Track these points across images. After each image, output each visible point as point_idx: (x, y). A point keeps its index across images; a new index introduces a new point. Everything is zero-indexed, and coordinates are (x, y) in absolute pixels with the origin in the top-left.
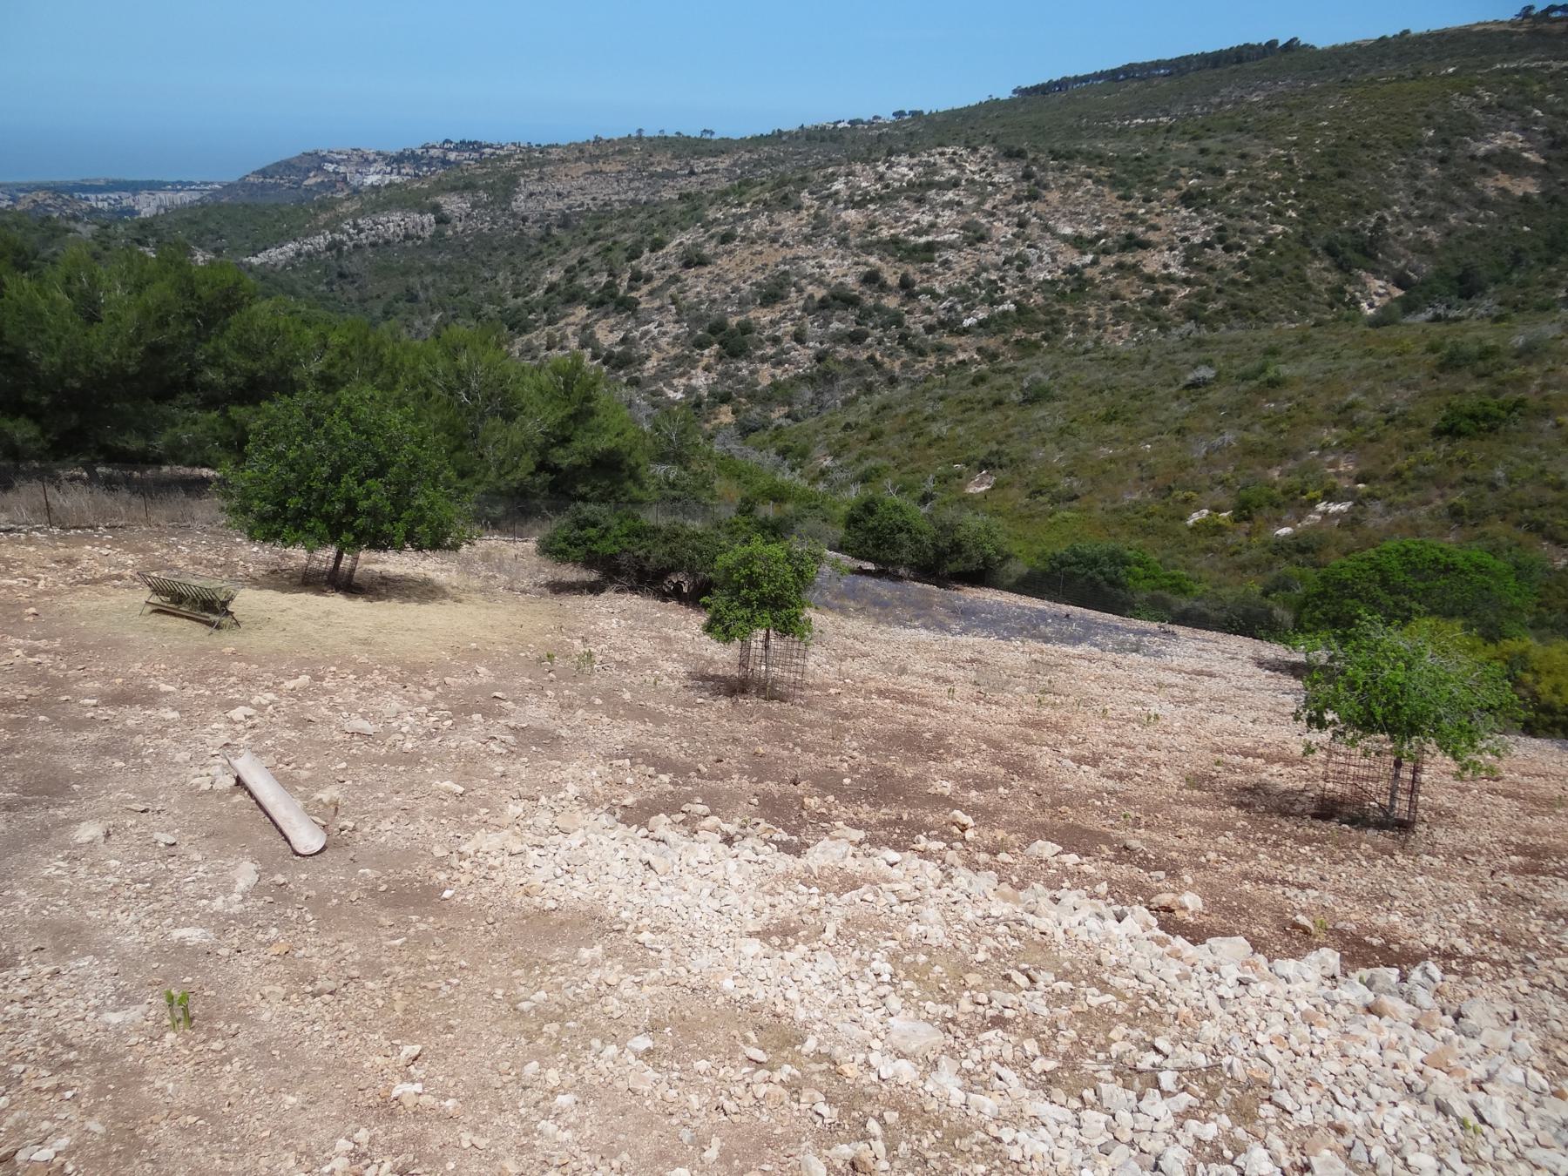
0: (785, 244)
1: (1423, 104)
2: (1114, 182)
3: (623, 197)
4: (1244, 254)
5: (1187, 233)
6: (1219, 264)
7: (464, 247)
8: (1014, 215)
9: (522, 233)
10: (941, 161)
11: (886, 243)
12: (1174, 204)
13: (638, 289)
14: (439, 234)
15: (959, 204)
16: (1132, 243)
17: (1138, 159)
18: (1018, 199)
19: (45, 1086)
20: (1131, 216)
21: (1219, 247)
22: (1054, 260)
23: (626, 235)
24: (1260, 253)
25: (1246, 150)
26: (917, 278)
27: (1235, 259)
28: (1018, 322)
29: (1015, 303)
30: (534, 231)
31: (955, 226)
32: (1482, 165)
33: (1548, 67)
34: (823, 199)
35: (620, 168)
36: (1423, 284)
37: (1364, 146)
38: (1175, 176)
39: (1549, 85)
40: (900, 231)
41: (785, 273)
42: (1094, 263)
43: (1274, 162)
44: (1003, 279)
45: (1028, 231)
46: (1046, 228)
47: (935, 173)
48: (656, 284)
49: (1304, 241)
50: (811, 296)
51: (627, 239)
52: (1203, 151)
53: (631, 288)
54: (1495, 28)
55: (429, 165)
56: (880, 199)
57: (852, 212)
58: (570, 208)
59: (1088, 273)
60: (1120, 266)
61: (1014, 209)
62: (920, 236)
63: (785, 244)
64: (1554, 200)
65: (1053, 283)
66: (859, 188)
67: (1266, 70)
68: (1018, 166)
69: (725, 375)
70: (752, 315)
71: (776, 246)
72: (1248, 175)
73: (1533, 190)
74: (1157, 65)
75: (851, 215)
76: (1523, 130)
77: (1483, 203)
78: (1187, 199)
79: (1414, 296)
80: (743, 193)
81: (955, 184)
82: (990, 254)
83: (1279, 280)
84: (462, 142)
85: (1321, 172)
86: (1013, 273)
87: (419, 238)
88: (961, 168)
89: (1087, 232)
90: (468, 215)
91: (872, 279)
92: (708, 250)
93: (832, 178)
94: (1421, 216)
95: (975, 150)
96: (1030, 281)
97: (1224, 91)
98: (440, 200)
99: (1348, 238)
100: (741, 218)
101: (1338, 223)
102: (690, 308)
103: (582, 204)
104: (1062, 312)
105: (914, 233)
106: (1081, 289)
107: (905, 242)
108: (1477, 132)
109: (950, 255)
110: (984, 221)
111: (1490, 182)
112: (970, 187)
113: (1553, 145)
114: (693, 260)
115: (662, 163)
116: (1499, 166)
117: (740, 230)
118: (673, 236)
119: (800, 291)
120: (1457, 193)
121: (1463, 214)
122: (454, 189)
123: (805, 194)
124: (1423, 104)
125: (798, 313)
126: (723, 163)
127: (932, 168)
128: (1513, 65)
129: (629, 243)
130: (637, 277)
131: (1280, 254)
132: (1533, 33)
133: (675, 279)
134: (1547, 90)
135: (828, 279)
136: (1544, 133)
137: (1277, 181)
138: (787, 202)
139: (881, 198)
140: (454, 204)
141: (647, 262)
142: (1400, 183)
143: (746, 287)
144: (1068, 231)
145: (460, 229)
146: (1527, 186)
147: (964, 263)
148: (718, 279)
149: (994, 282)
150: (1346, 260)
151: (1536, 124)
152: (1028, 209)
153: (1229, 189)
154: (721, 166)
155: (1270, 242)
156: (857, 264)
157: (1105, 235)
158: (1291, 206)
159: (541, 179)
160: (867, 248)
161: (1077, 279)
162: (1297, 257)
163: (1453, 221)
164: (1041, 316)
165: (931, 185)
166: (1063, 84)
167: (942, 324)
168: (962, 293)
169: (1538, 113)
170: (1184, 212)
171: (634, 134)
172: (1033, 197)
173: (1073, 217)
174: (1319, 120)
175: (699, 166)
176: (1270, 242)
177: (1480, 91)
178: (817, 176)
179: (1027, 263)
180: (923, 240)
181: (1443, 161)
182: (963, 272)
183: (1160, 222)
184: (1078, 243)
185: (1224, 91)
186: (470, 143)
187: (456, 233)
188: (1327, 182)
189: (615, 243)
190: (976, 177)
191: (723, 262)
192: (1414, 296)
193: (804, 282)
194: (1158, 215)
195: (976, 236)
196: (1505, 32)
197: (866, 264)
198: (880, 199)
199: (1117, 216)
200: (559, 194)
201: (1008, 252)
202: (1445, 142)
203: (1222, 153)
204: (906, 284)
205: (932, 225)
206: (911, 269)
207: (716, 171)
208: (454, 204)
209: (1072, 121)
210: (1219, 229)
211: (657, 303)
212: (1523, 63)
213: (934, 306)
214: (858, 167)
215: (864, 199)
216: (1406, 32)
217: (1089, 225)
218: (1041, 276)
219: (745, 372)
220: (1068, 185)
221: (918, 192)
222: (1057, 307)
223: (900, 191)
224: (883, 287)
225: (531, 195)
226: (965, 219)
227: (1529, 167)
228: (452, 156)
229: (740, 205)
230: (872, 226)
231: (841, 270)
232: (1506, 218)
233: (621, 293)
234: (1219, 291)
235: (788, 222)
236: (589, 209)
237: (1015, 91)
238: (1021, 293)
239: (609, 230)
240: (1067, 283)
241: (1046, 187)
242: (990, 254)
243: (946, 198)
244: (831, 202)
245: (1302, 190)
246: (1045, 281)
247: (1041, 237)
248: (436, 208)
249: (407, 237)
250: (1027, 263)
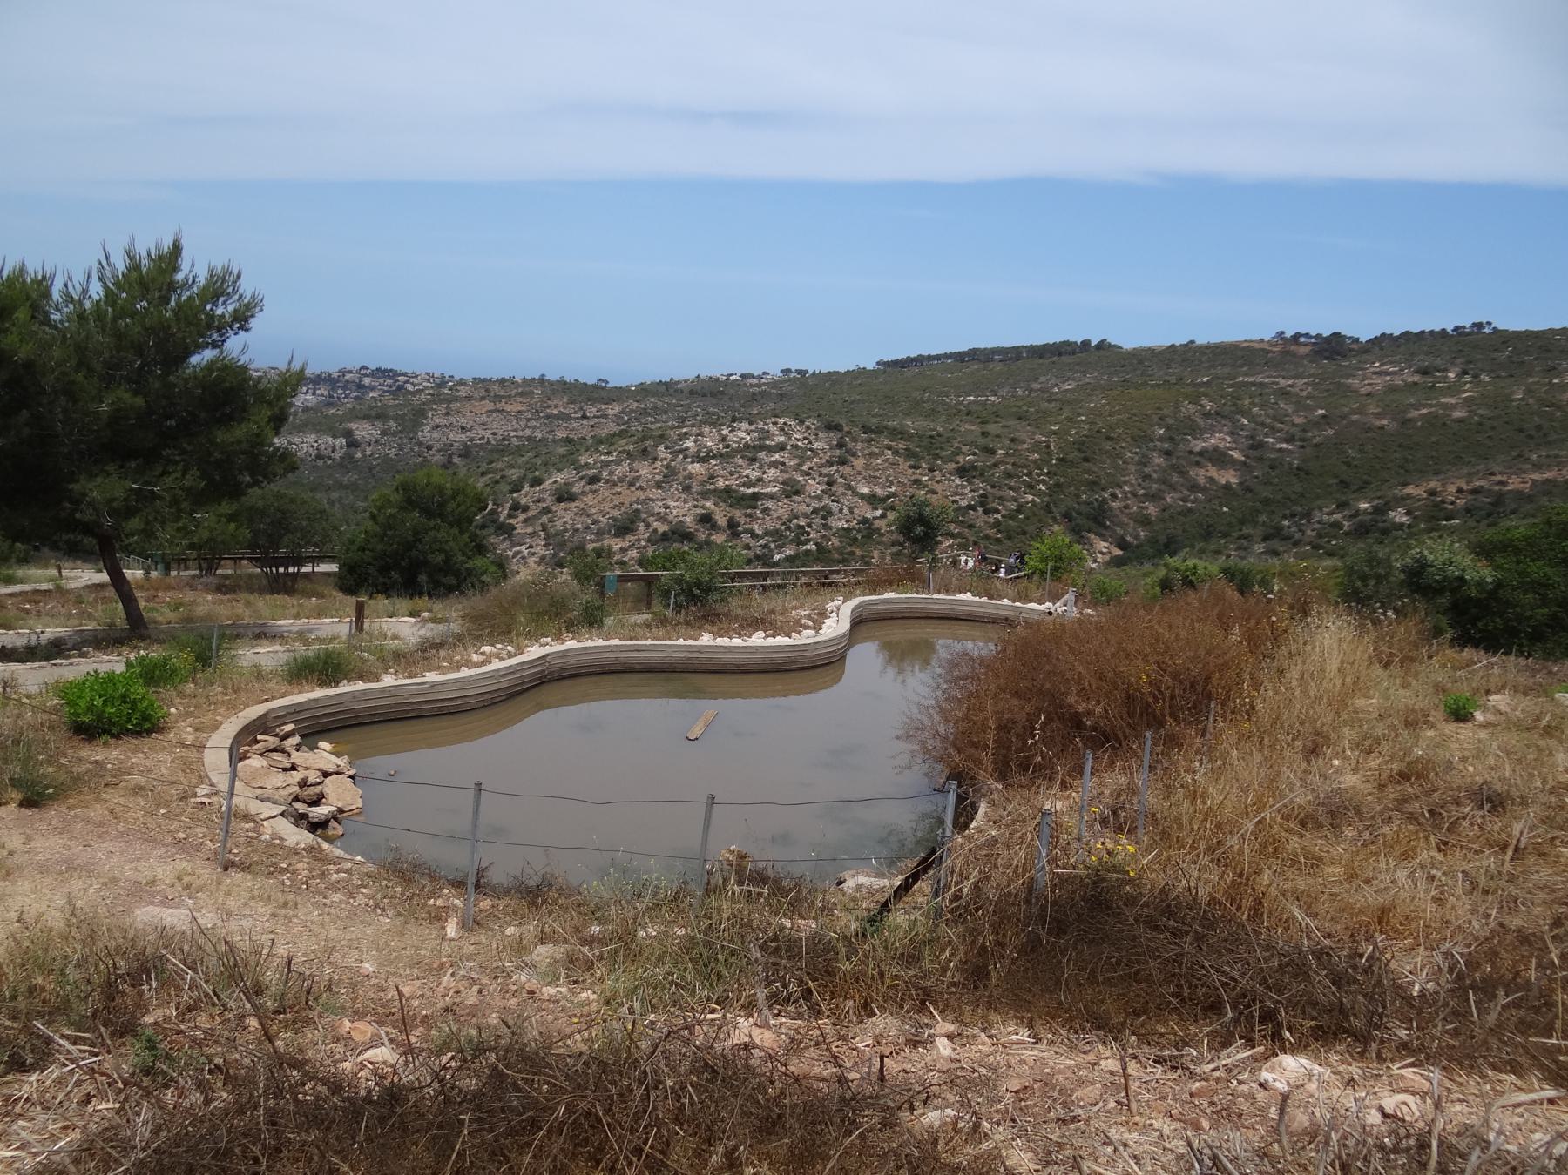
0: (640, 488)
1: (1159, 408)
2: (909, 454)
3: (520, 433)
4: (999, 516)
5: (958, 498)
6: (979, 523)
7: (371, 469)
8: (826, 475)
9: (425, 460)
10: (773, 429)
11: (721, 491)
12: (951, 474)
13: (516, 517)
14: (349, 456)
15: (783, 464)
17: (931, 437)
18: (830, 463)
20: (916, 482)
21: (980, 509)
22: (852, 513)
23: (512, 471)
24: (1011, 516)
25: (1018, 435)
26: (742, 521)
27: (992, 520)
28: (818, 560)
29: (816, 544)
30: (437, 458)
31: (777, 481)
32: (1197, 459)
33: (1277, 383)
34: (676, 454)
35: (520, 408)
36: (1137, 547)
37: (1108, 438)
38: (958, 452)
39: (1257, 401)
40: (733, 483)
41: (637, 511)
42: (883, 516)
43: (1036, 447)
44: (809, 525)
45: (834, 489)
46: (849, 487)
47: (767, 438)
48: (531, 513)
49: (1047, 509)
50: (655, 531)
51: (514, 474)
52: (985, 434)
53: (510, 516)
54: (1257, 346)
55: (344, 388)
56: (721, 456)
57: (697, 465)
58: (471, 440)
59: (877, 524)
61: (825, 470)
62: (748, 488)
63: (640, 488)
64: (1248, 490)
65: (848, 530)
66: (705, 446)
67: (1078, 364)
68: (834, 437)
70: (606, 543)
71: (633, 489)
72: (1013, 455)
73: (1234, 481)
74: (995, 351)
75: (696, 468)
76: (1232, 434)
77: (1194, 487)
78: (962, 471)
79: (1130, 554)
80: (612, 444)
81: (781, 448)
82: (802, 505)
83: (1023, 538)
84: (378, 370)
85: (1071, 457)
86: (818, 521)
87: (330, 458)
88: (788, 435)
89: (880, 492)
90: (377, 441)
91: (706, 519)
92: (576, 489)
93: (685, 436)
94: (1145, 495)
95: (802, 422)
96: (830, 528)
97: (1043, 379)
98: (353, 426)
99: (1084, 509)
100: (606, 464)
101: (1078, 496)
102: (556, 534)
103: (483, 438)
104: (853, 553)
105: (744, 485)
106: (869, 536)
107: (735, 491)
108: (1195, 431)
109: (770, 504)
110: (800, 479)
111: (1202, 472)
112: (794, 451)
113: (1252, 447)
114: (564, 496)
115: (559, 406)
116: (1210, 460)
117: (605, 474)
118: (550, 476)
119: (648, 526)
120: (1175, 478)
121: (1176, 496)
122: (366, 417)
123: (661, 448)
124: (1159, 408)
125: (643, 543)
126: (612, 410)
127: (765, 434)
128: (1252, 379)
129: (514, 477)
130: (516, 507)
131: (1027, 518)
132: (1285, 353)
133: (547, 511)
134: (1254, 405)
135: (670, 517)
136: (1247, 437)
137: (1035, 461)
138: (646, 454)
139: (721, 455)
140: (365, 431)
141: (526, 496)
142: (1132, 468)
143: (604, 520)
144: (866, 490)
145: (368, 453)
146: (1230, 477)
147: (780, 511)
148: (582, 512)
149: (803, 527)
150: (1077, 525)
151: (1242, 430)
152: (837, 471)
153: (995, 465)
154: (610, 412)
155: (1020, 508)
156: (696, 507)
157: (894, 495)
158: (1043, 482)
159: (448, 414)
160: (705, 495)
161: (869, 528)
162: (1040, 521)
163: (1169, 500)
164: (836, 556)
165: (762, 448)
166: (918, 361)
167: (757, 558)
168: (776, 535)
169: (1245, 421)
170: (958, 481)
171: (537, 377)
172: (843, 462)
173: (871, 480)
174: (1079, 415)
175: (591, 411)
176: (1020, 508)
177: (1204, 401)
178: (673, 434)
179: (830, 513)
180: (750, 491)
181: (1168, 453)
182: (779, 518)
183: (938, 488)
184: (873, 500)
185: (1043, 379)
186: (386, 370)
187: (365, 456)
188: (1072, 464)
189: (503, 477)
190: (800, 444)
191: (588, 499)
192: (1130, 554)
193: (651, 518)
194: (938, 482)
195: (792, 490)
196: (1263, 350)
197: (703, 507)
198: (721, 456)
199: (906, 481)
200: (463, 428)
201: (816, 504)
202: (1172, 439)
203: (998, 436)
204: (732, 525)
205: (759, 480)
206: (738, 514)
207: (606, 416)
208: (365, 431)
209: (917, 394)
210: (982, 496)
211: (530, 530)
212: (1259, 379)
213: (752, 543)
214: (707, 429)
215: (708, 456)
216: (1192, 342)
217: (883, 487)
218: (840, 524)
220: (872, 454)
221: (751, 453)
222: (849, 549)
223: (738, 450)
224: (714, 526)
225: (437, 427)
226: (786, 476)
227: (1233, 461)
228: (367, 381)
229: (609, 453)
230: (712, 477)
231: (682, 510)
232: (1210, 501)
233: (501, 519)
234: (975, 543)
235: (645, 470)
236: (488, 443)
237: (878, 363)
238: (823, 537)
239: (500, 465)
240: (859, 531)
241: (854, 455)
242: (802, 505)
243: (773, 459)
244: (681, 456)
245: (1053, 469)
246: (843, 528)
247: (844, 494)
248: (348, 434)
249: (319, 457)
250: (830, 513)
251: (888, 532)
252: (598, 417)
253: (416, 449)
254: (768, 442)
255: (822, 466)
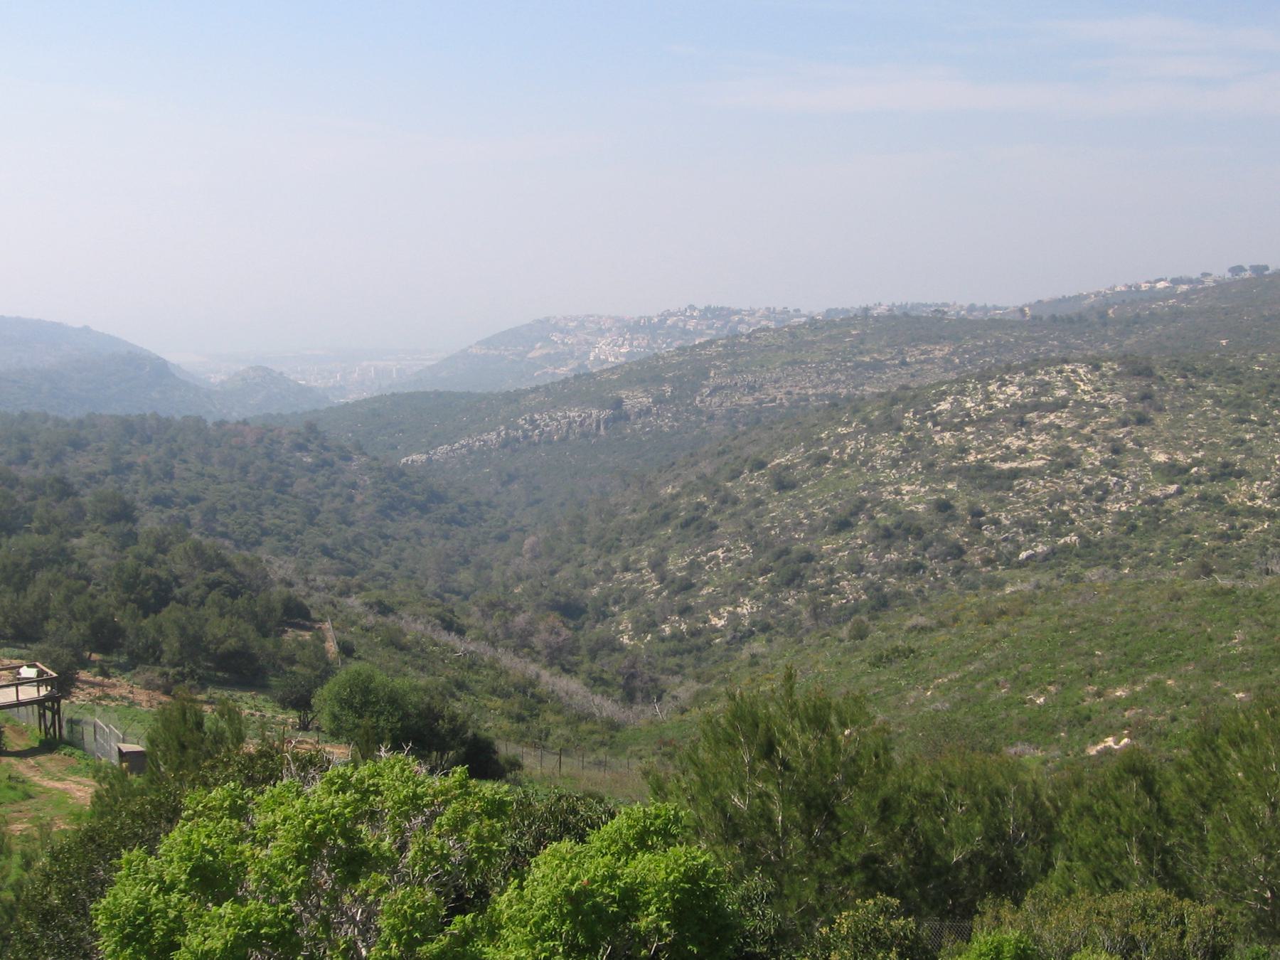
2: (1241, 404)
8: (1113, 440)
16: (1226, 472)
19: (43, 576)
29: (1080, 536)
58: (760, 402)
60: (1203, 498)
68: (1139, 384)
69: (774, 604)
81: (1060, 405)
84: (708, 309)
103: (774, 400)
126: (940, 352)
145: (638, 427)
172: (1142, 420)
179: (1107, 492)
180: (1006, 466)
195: (1064, 461)
205: (1023, 451)
219: (791, 602)
224: (953, 518)
236: (781, 405)
241: (1160, 410)
242: (1071, 482)
243: (1046, 421)
250: (1107, 492)
251: (1181, 515)
252: (922, 362)
253: (693, 418)
254: (1043, 399)
255: (1110, 426)
